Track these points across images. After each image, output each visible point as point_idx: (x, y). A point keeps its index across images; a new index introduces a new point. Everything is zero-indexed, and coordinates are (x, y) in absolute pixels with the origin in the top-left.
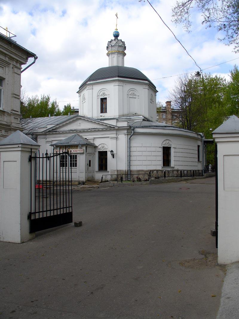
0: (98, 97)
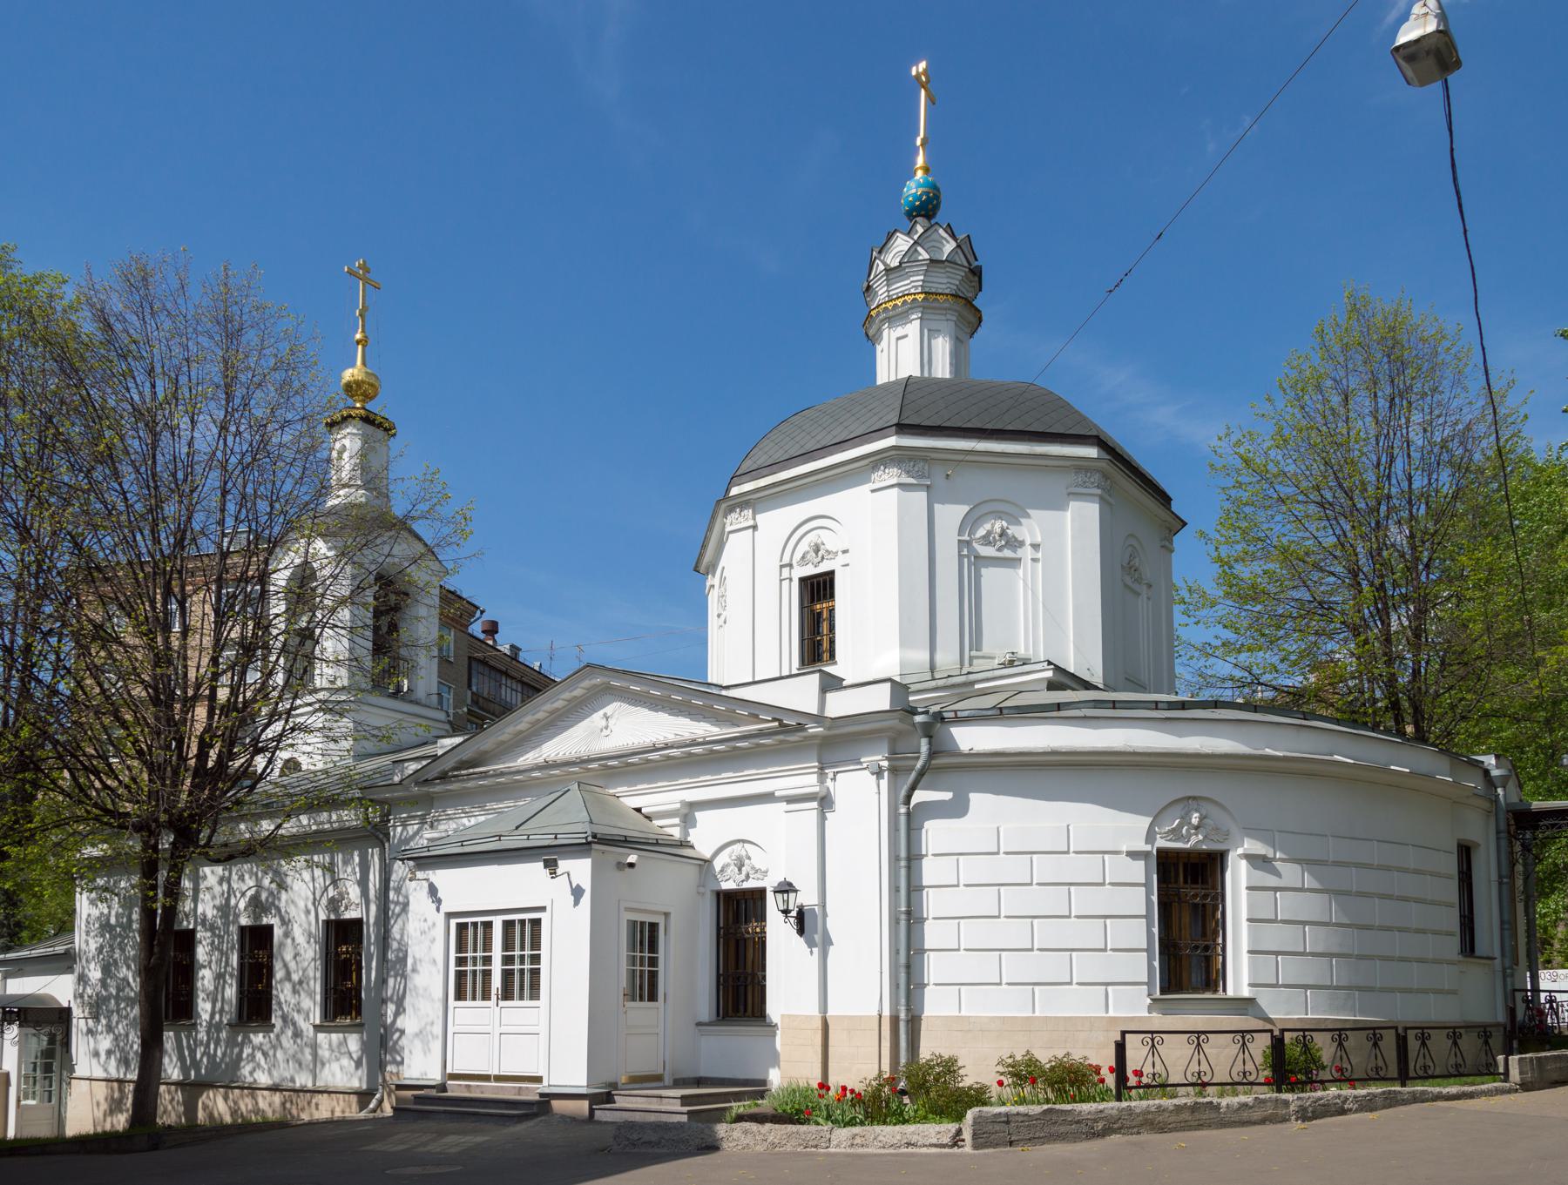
0: (786, 571)
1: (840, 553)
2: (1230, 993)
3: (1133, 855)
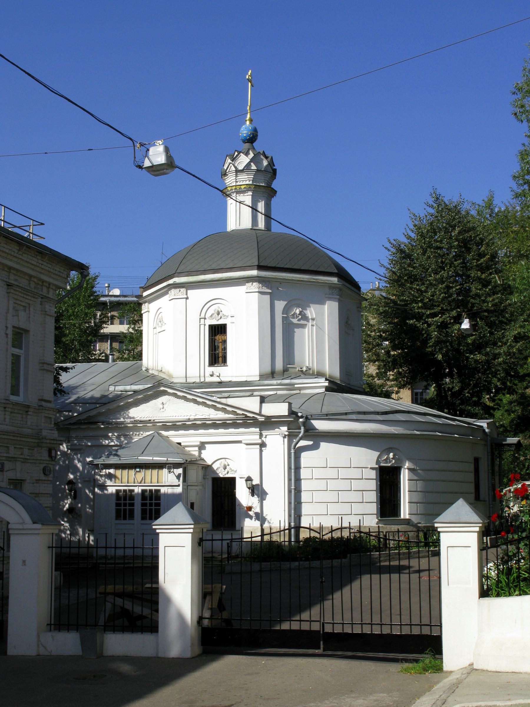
1: (229, 317)
2: (402, 517)
3: (372, 468)
